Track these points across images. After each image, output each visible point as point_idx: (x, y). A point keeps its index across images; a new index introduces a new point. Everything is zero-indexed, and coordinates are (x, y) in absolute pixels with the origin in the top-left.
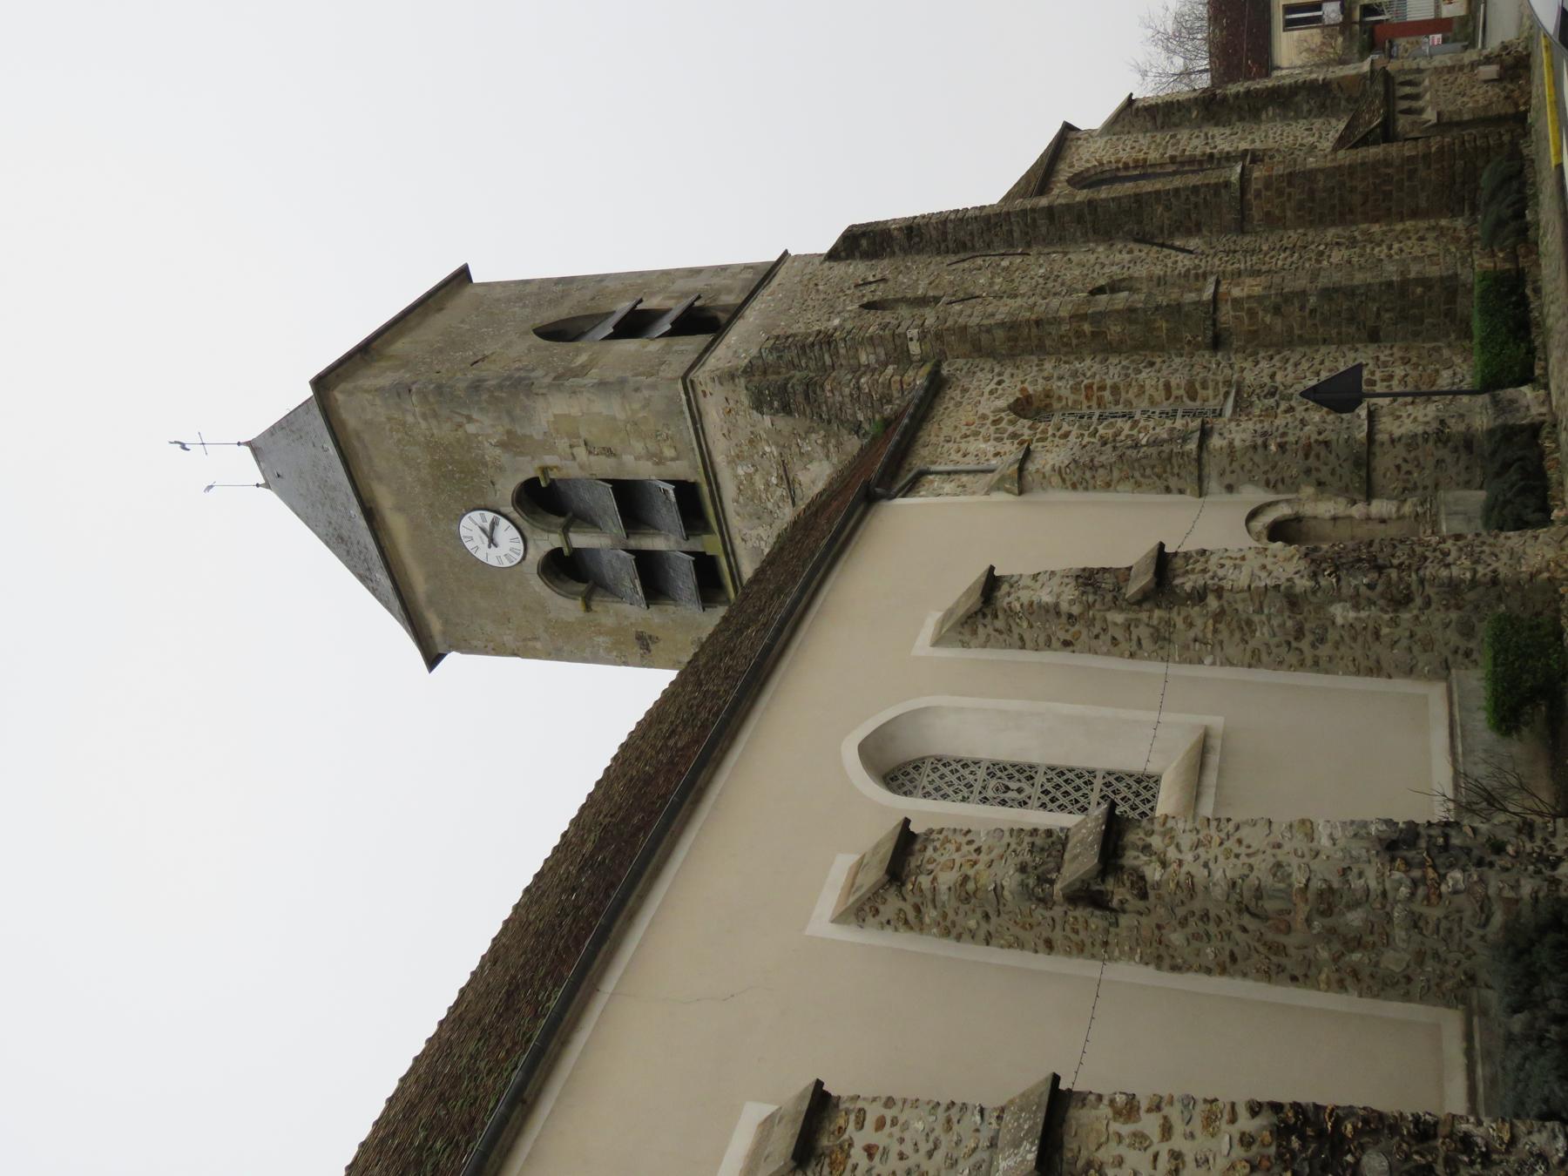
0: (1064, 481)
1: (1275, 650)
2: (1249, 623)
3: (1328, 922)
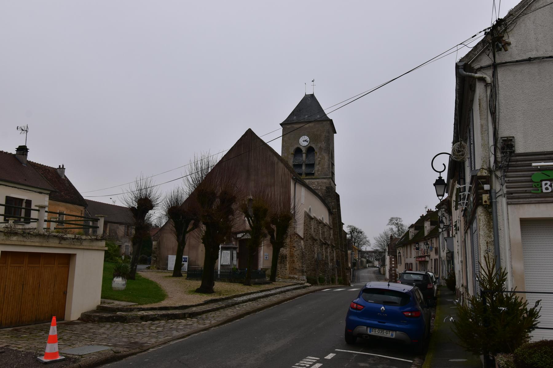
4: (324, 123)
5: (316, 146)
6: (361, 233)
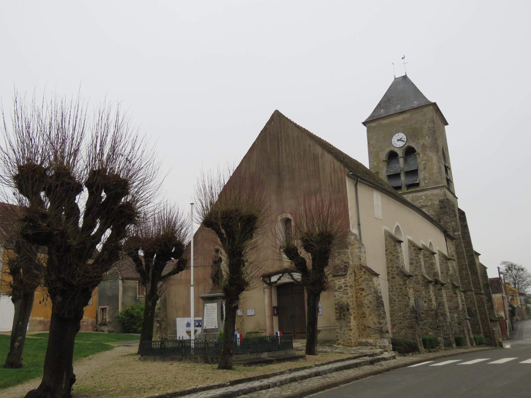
4: (425, 110)
5: (417, 144)
6: (522, 270)
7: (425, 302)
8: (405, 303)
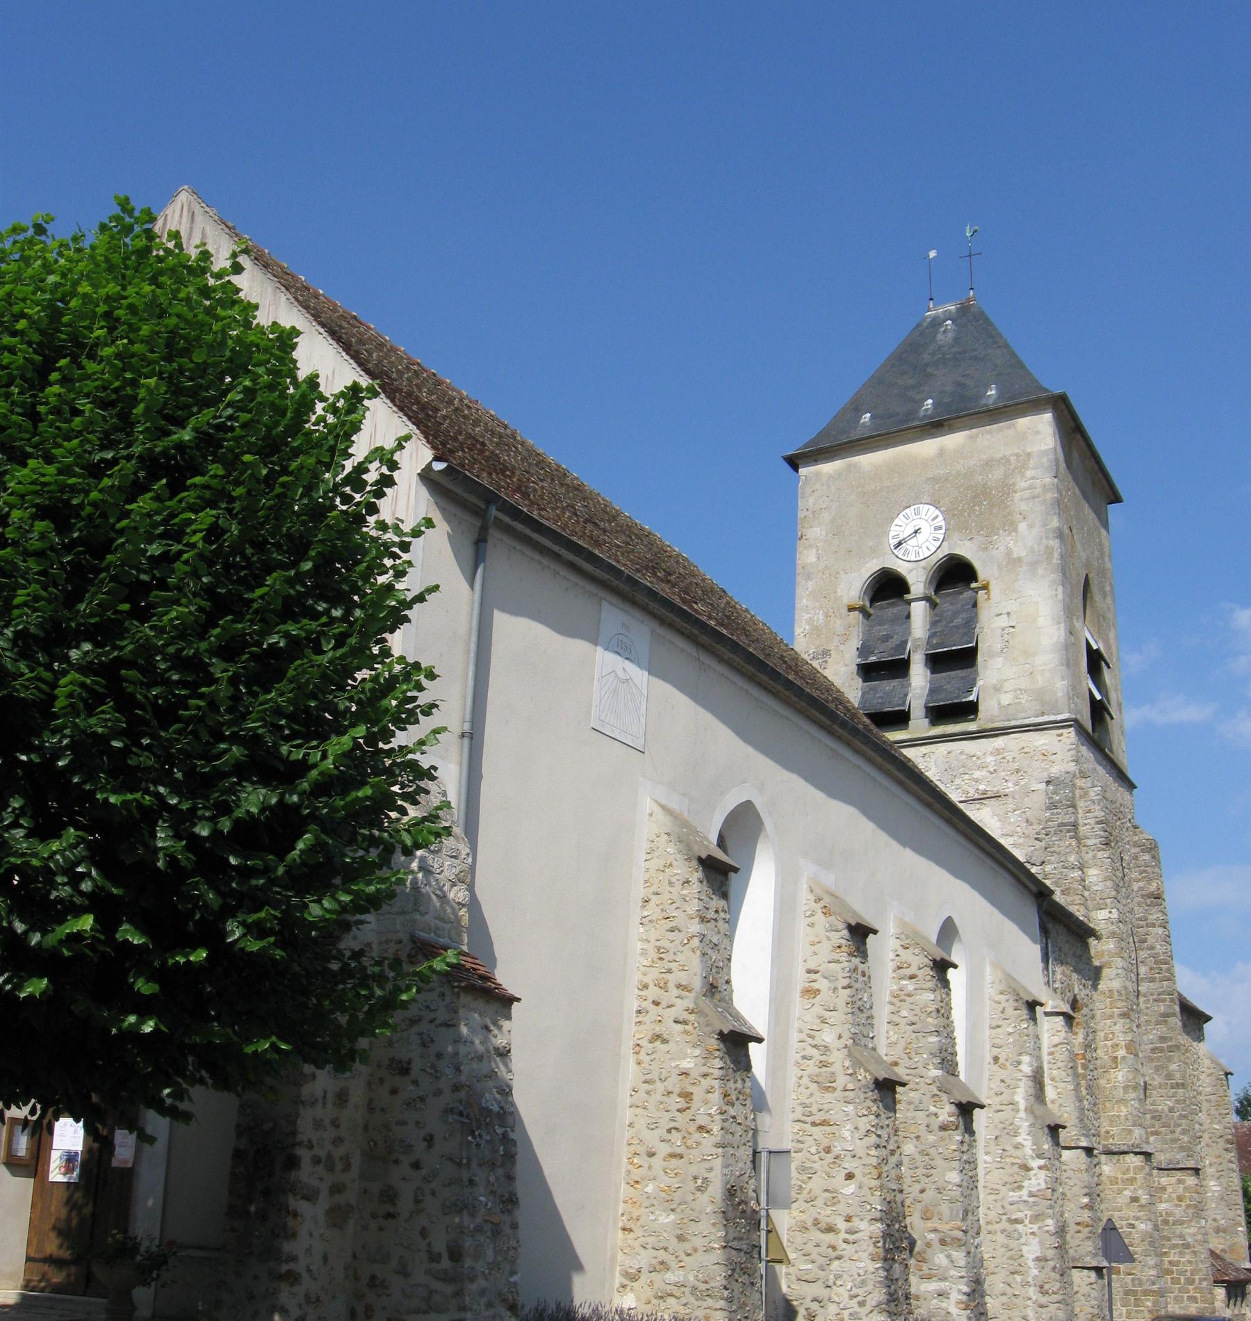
0: (1055, 1046)
1: (999, 1204)
2: (1020, 1188)
3: (936, 1244)
7: (850, 1176)
8: (693, 1170)
